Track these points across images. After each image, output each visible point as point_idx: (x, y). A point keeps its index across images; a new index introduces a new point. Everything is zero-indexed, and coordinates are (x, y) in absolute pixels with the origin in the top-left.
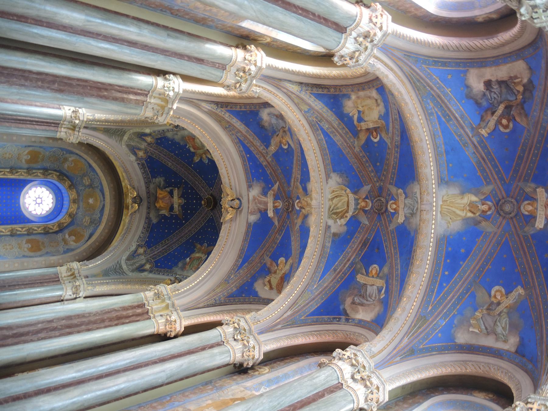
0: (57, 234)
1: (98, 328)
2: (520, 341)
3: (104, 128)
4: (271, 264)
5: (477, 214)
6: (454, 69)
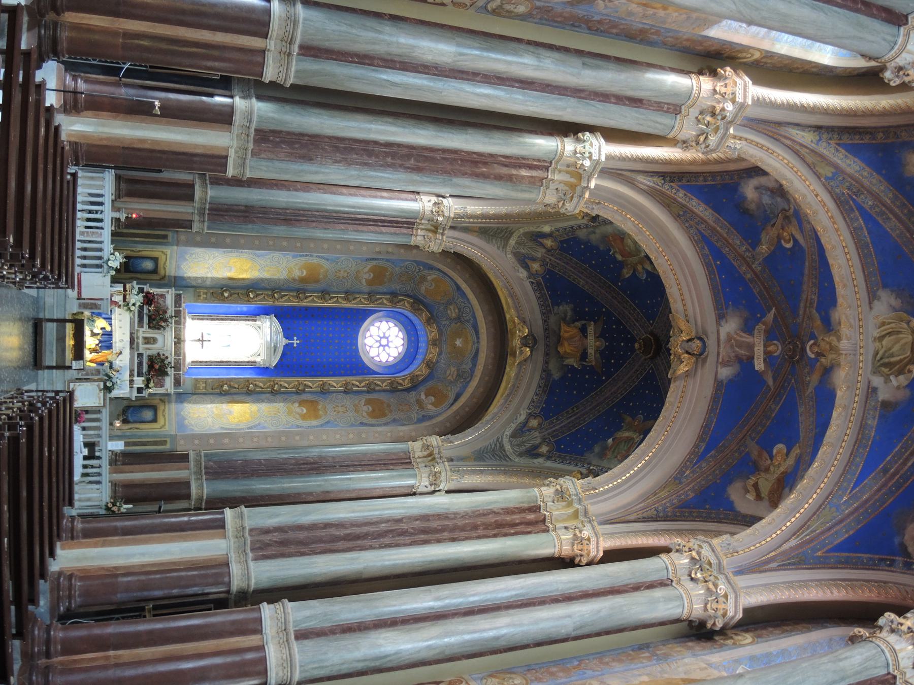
0: (409, 392)
1: (467, 538)
3: (480, 228)
4: (760, 455)
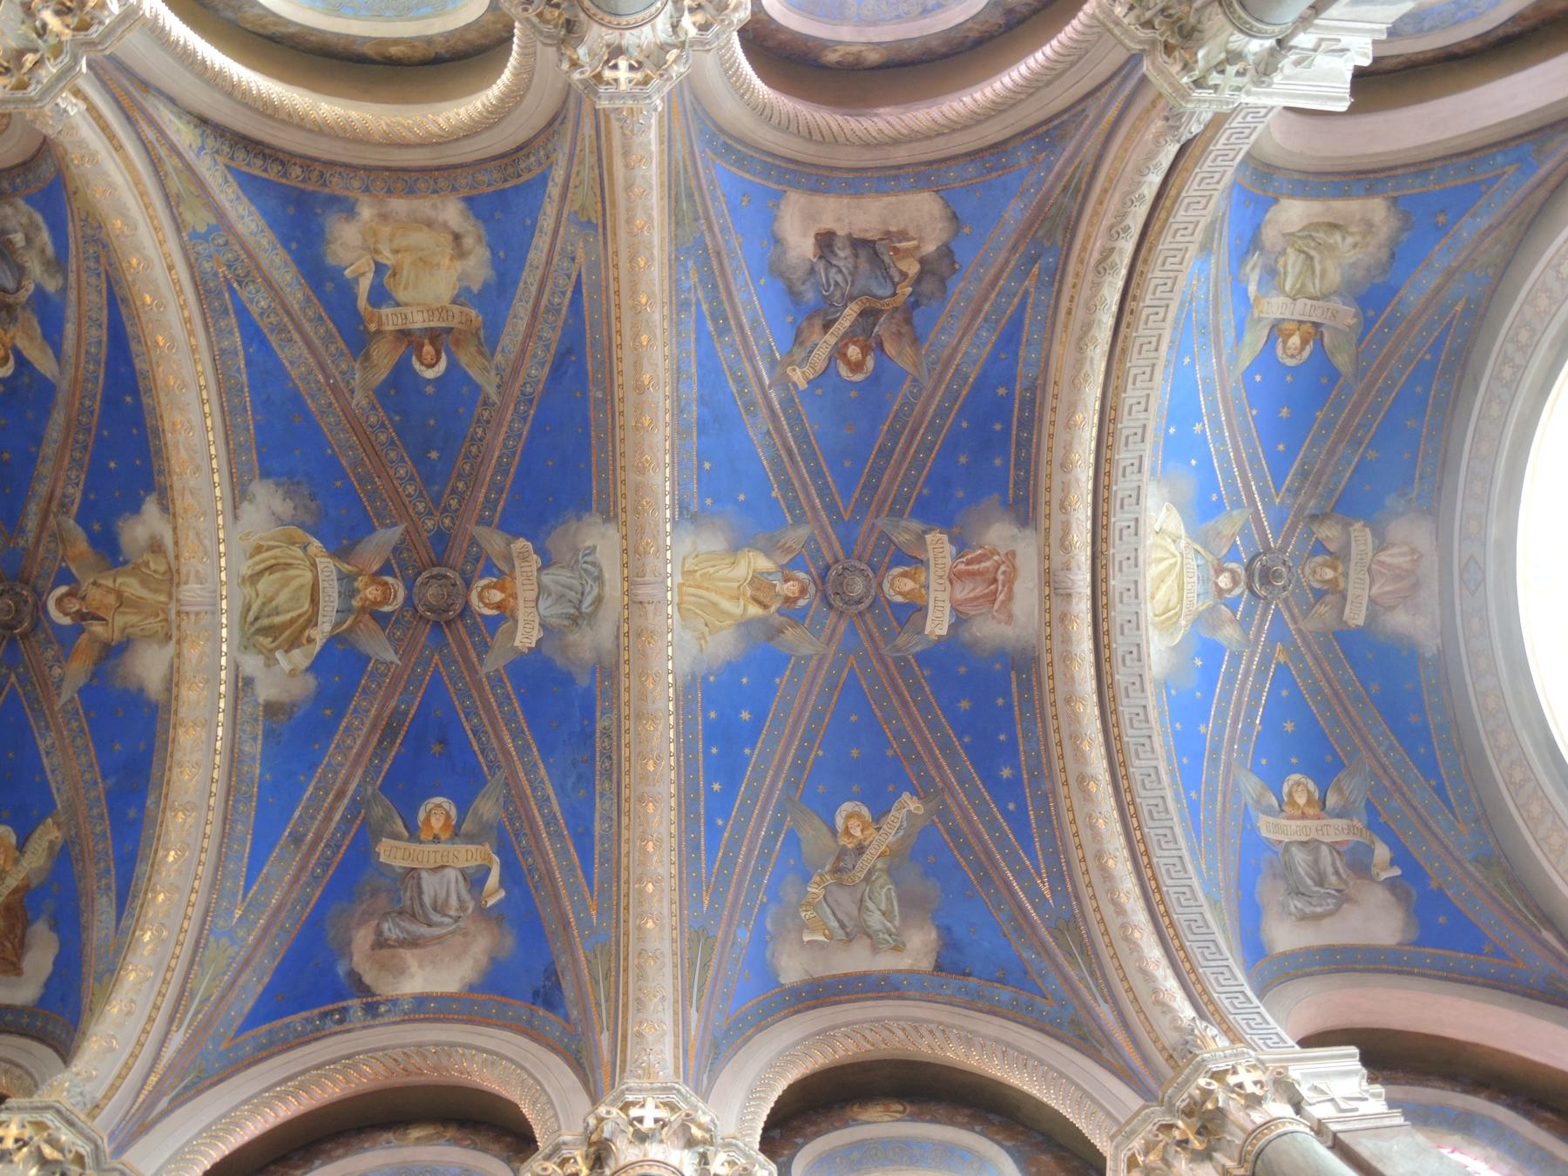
2: (940, 937)
5: (773, 609)
6: (758, 181)
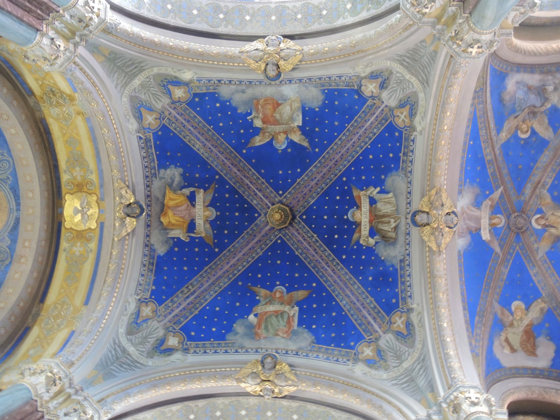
4: (503, 313)
